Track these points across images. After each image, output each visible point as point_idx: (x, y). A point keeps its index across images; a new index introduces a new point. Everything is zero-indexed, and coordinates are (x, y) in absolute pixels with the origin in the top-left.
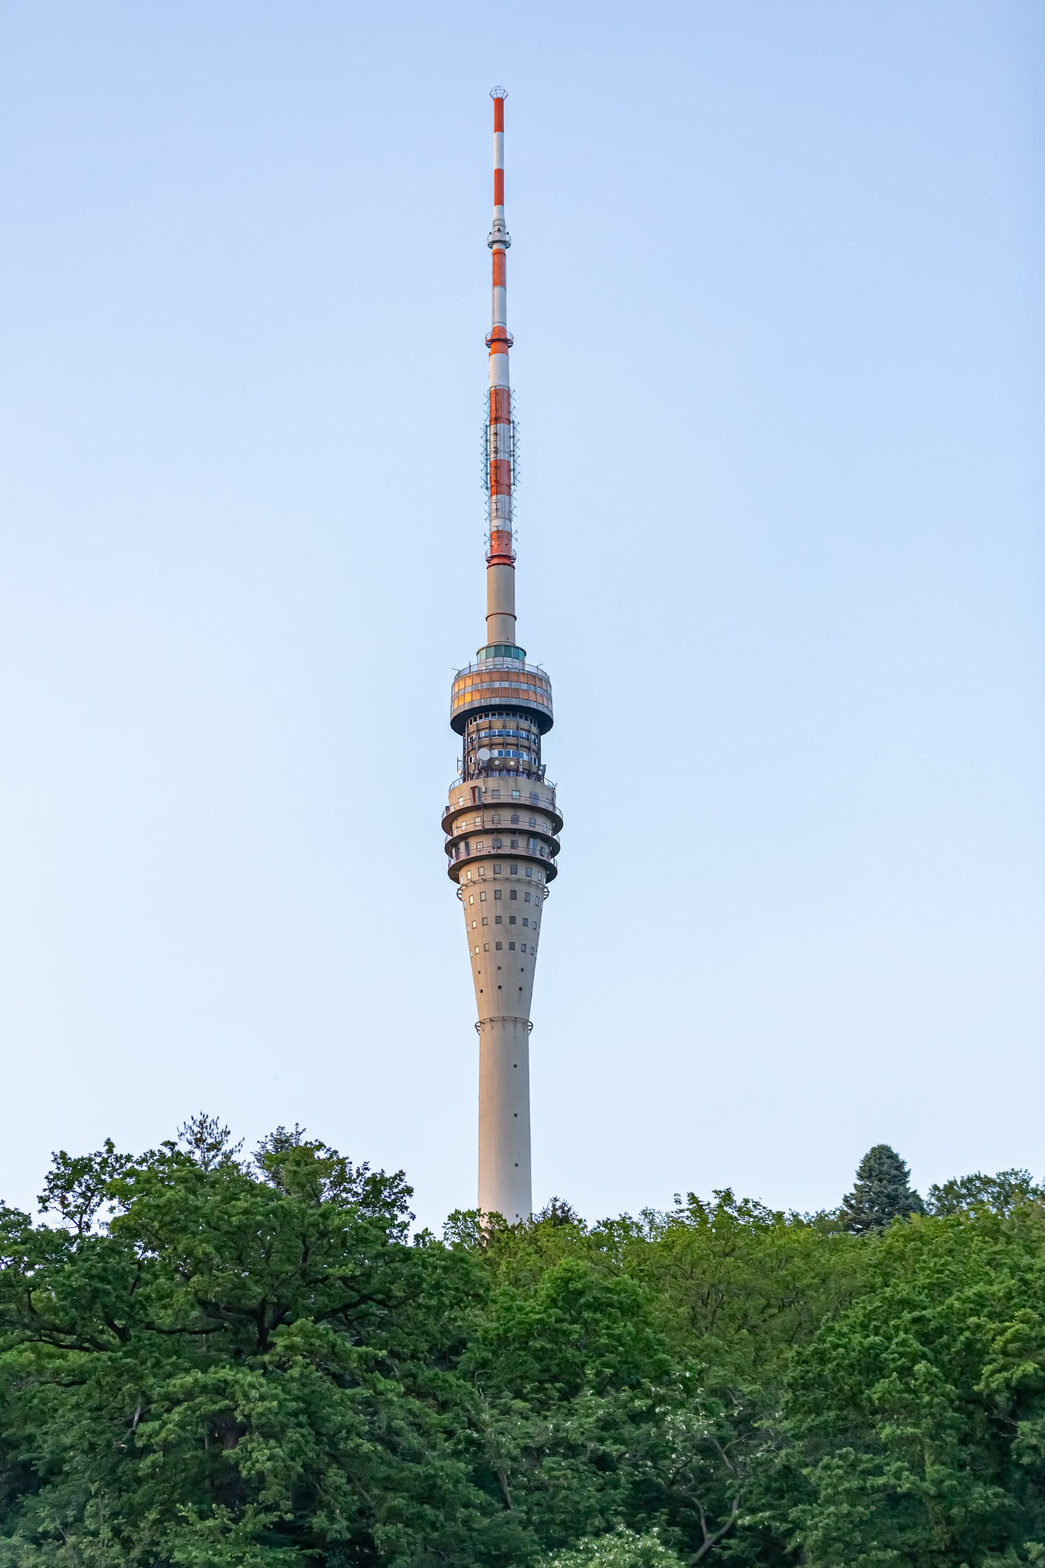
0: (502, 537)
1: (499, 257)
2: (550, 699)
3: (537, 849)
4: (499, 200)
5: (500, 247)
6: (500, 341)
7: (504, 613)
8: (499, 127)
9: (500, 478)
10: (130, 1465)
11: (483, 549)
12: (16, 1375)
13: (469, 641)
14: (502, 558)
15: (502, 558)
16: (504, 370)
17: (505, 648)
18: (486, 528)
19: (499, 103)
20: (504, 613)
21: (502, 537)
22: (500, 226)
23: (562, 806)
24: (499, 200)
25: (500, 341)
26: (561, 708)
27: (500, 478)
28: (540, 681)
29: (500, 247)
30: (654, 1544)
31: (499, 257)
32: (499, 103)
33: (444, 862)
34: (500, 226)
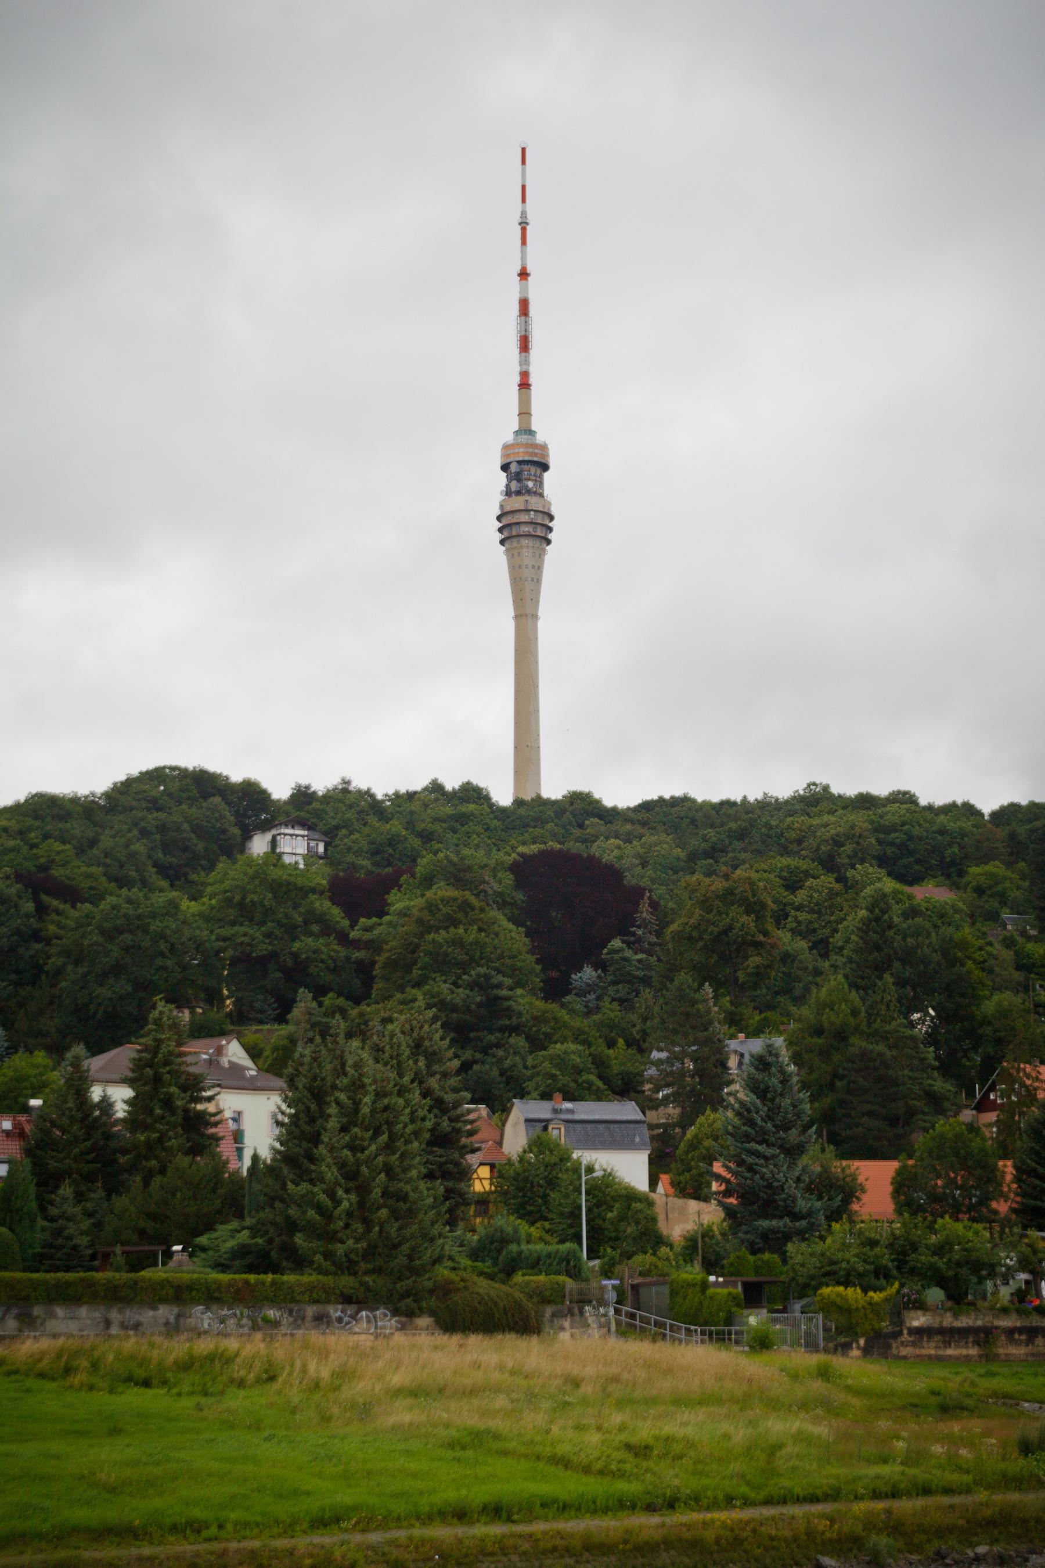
0: (525, 376)
1: (524, 231)
2: (548, 456)
3: (540, 532)
4: (524, 200)
5: (524, 225)
6: (524, 274)
7: (525, 413)
8: (524, 162)
9: (525, 345)
10: (943, 1547)
11: (517, 379)
12: (1036, 940)
13: (507, 429)
14: (525, 385)
15: (525, 385)
16: (524, 289)
17: (525, 430)
18: (517, 369)
19: (524, 150)
20: (525, 413)
21: (525, 376)
22: (524, 214)
23: (554, 511)
24: (524, 200)
25: (524, 274)
26: (552, 462)
27: (525, 345)
28: (544, 447)
29: (524, 225)
30: (328, 1166)
31: (524, 231)
32: (524, 150)
33: (499, 536)
34: (524, 214)
